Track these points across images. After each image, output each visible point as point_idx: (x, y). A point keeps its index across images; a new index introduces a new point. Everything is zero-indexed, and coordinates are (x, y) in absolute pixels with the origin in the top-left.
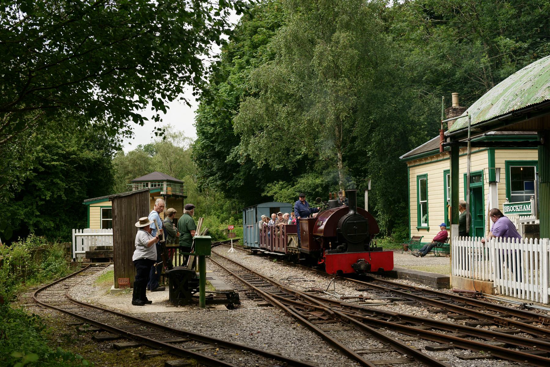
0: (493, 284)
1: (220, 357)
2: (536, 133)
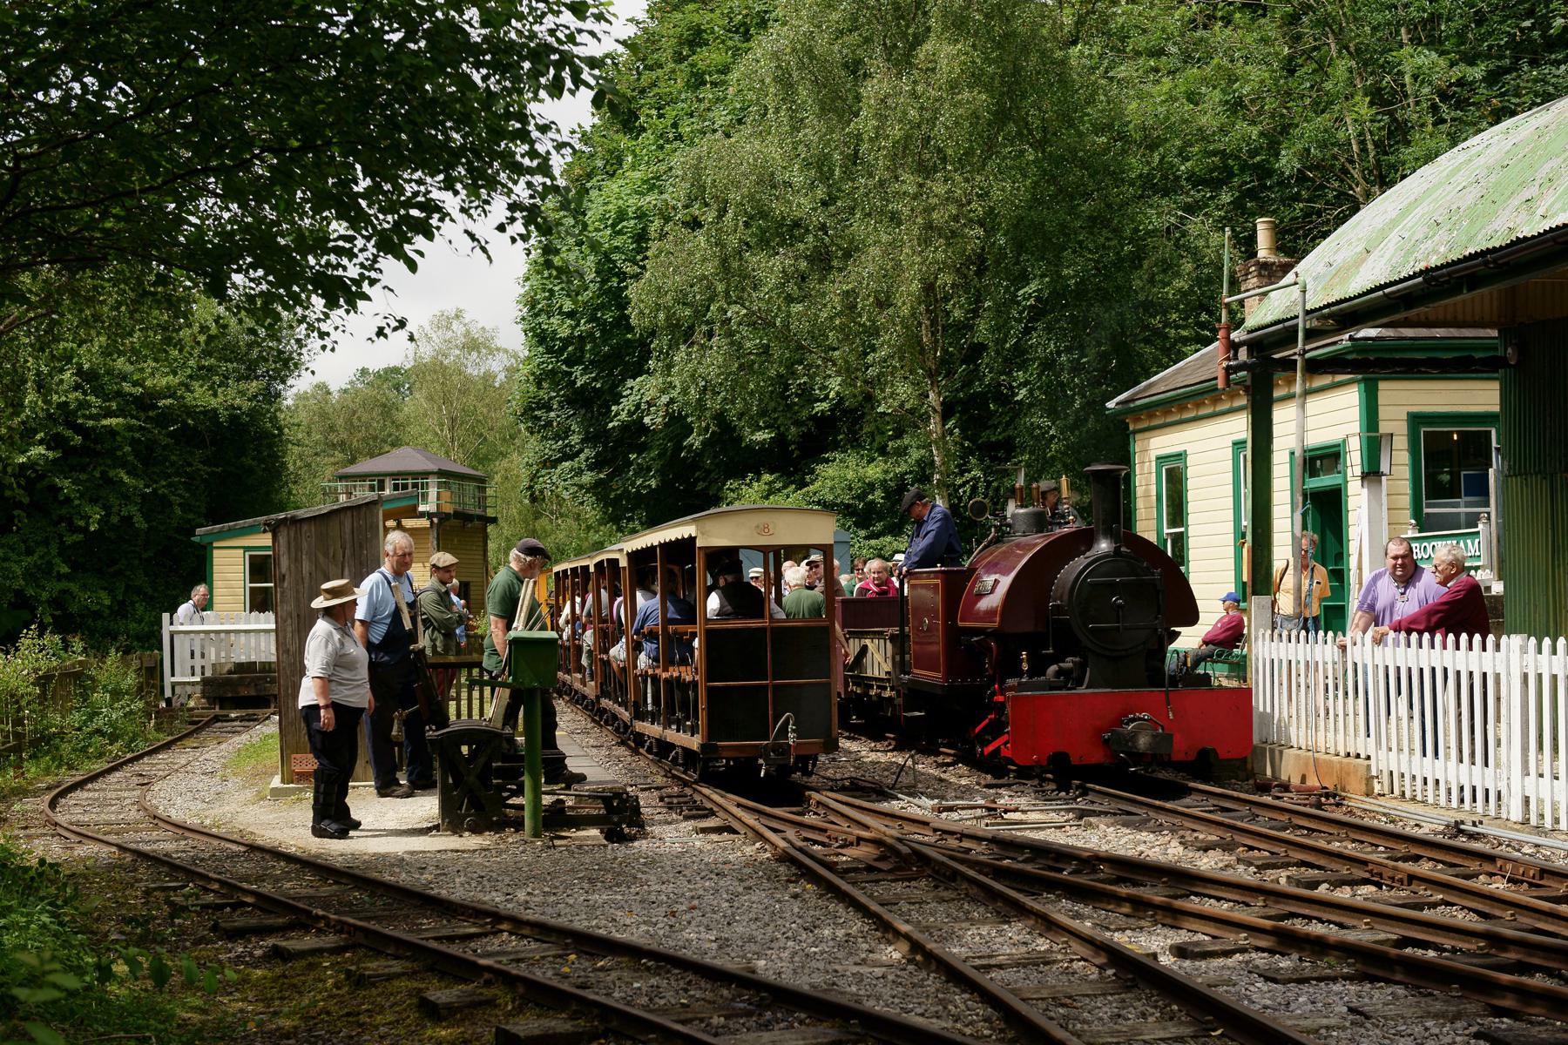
0: (1369, 767)
1: (580, 980)
2: (1495, 333)
